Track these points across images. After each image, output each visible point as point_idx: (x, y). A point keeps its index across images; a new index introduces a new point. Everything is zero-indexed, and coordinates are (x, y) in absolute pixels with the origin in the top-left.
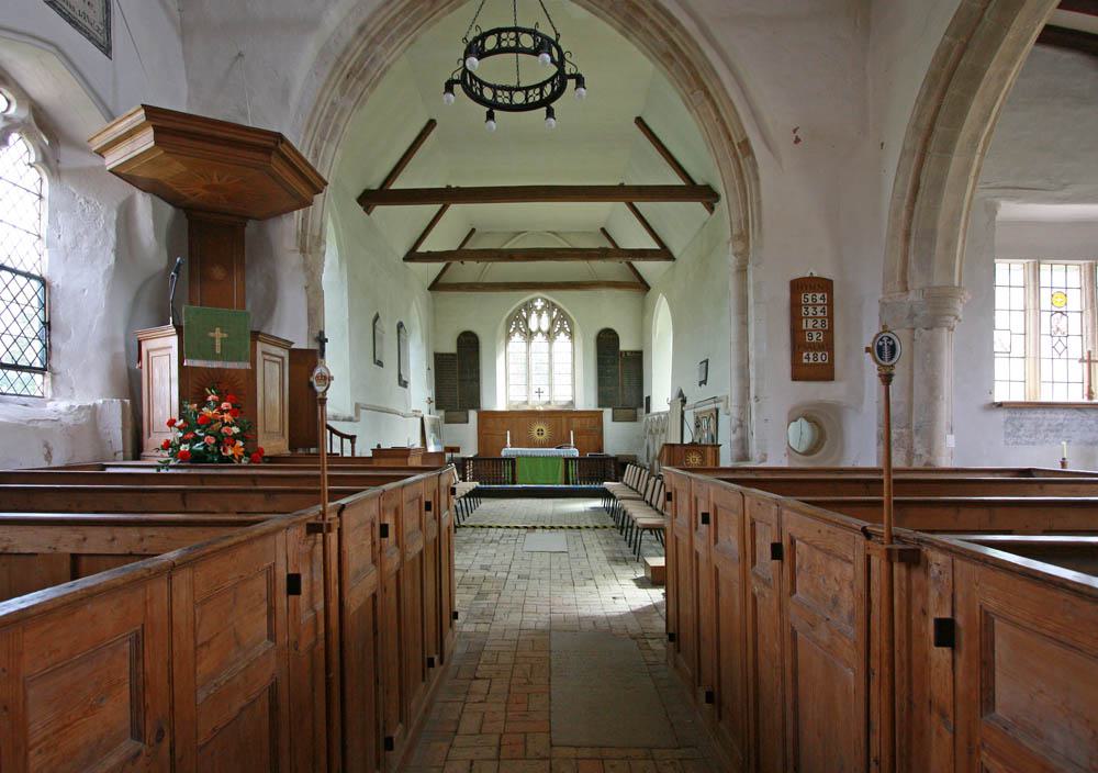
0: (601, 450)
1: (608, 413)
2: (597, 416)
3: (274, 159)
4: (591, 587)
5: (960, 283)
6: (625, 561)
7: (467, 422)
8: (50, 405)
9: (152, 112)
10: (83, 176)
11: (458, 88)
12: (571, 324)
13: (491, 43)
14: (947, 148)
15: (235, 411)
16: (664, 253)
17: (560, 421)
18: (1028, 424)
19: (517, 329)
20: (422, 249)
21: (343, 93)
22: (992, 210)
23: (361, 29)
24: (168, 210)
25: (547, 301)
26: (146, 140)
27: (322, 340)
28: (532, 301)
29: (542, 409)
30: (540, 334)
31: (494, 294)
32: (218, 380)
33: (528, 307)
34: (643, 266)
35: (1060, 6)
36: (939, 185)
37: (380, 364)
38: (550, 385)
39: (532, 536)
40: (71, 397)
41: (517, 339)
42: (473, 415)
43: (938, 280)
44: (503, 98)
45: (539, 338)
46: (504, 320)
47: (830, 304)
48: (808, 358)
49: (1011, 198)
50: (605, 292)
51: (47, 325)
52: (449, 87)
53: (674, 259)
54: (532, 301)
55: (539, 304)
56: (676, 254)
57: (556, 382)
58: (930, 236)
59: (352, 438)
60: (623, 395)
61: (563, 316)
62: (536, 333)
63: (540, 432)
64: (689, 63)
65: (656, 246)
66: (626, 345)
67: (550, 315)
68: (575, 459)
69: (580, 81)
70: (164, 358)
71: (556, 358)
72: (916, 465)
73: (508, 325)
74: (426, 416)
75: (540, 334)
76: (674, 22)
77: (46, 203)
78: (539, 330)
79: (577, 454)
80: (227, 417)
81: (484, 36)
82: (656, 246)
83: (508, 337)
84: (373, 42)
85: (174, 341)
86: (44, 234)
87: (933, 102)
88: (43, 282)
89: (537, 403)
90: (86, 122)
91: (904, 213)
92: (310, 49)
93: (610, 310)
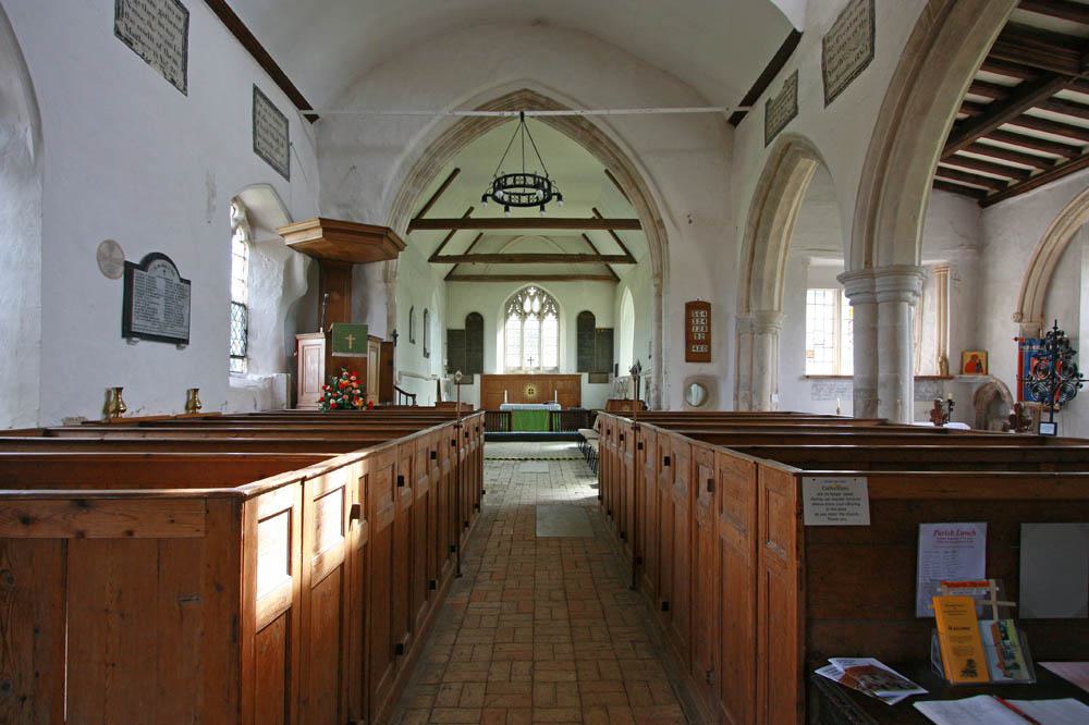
0: (579, 406)
1: (585, 377)
2: (576, 379)
3: (385, 241)
4: (563, 488)
5: (780, 307)
6: (588, 477)
7: (472, 383)
8: (249, 377)
9: (322, 221)
10: (271, 246)
11: (489, 199)
12: (557, 307)
13: (510, 181)
14: (766, 236)
15: (357, 381)
16: (628, 258)
17: (547, 383)
18: (825, 388)
19: (514, 310)
20: (441, 254)
21: (414, 185)
22: (806, 263)
23: (427, 150)
24: (309, 259)
25: (539, 289)
26: (317, 235)
27: (395, 336)
28: (526, 289)
29: (532, 373)
30: (532, 315)
31: (498, 284)
32: (345, 363)
33: (524, 293)
34: (615, 266)
35: (1019, 6)
36: (763, 256)
37: (413, 342)
38: (540, 355)
39: (523, 464)
40: (257, 373)
41: (514, 319)
42: (477, 378)
43: (765, 307)
44: (515, 199)
45: (532, 317)
46: (503, 304)
47: (709, 318)
48: (696, 349)
49: (816, 256)
50: (585, 283)
51: (246, 331)
52: (484, 199)
53: (635, 262)
54: (526, 289)
55: (532, 291)
56: (638, 260)
57: (544, 352)
58: (760, 282)
59: (414, 396)
60: (597, 363)
61: (551, 301)
62: (529, 314)
63: (531, 391)
64: (628, 173)
65: (624, 254)
66: (600, 324)
67: (541, 300)
68: (558, 412)
69: (560, 198)
70: (314, 349)
71: (544, 333)
72: (754, 410)
73: (507, 306)
74: (442, 379)
75: (532, 315)
76: (618, 148)
77: (247, 263)
78: (532, 311)
79: (560, 409)
80: (354, 384)
81: (506, 177)
82: (624, 254)
83: (507, 317)
84: (435, 155)
85: (323, 342)
86: (245, 279)
87: (757, 210)
88: (243, 305)
89: (529, 368)
90: (277, 220)
91: (747, 268)
92: (398, 163)
93: (589, 297)
